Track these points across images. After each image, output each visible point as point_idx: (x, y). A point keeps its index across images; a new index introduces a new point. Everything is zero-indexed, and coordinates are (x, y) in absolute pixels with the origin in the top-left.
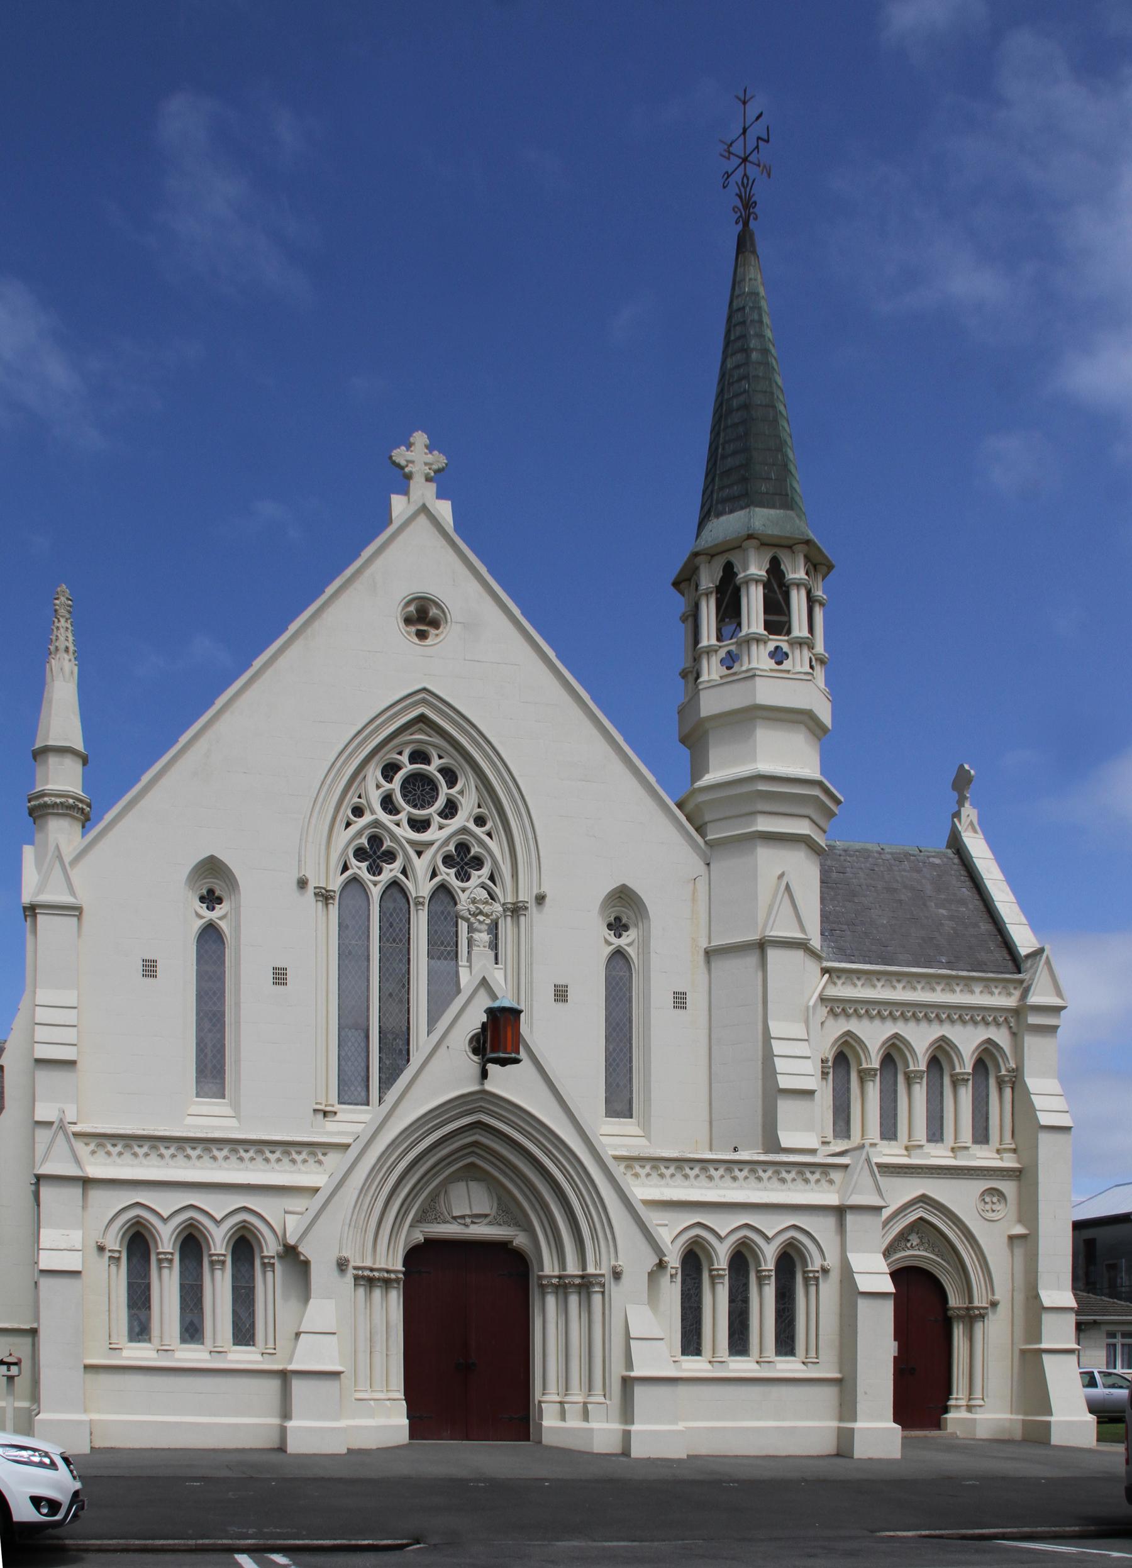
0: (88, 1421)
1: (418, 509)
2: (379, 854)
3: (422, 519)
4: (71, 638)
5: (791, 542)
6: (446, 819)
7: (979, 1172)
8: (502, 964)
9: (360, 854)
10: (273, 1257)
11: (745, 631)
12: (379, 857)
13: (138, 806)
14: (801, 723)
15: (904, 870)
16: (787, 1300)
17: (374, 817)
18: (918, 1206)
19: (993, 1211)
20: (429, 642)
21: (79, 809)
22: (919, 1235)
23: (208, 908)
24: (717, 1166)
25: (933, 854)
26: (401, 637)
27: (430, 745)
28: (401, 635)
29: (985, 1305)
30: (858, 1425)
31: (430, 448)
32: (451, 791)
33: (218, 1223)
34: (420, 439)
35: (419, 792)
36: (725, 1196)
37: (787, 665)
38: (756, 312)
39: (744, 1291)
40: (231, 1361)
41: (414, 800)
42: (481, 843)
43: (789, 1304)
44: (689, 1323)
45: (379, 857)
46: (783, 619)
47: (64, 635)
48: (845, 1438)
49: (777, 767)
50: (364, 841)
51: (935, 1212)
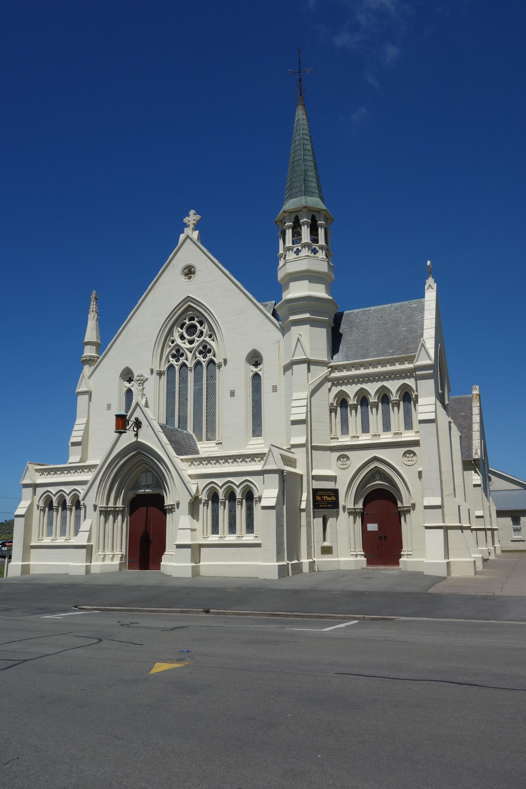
2: (179, 355)
3: (188, 240)
9: (174, 356)
12: (179, 356)
16: (251, 510)
17: (176, 342)
19: (411, 461)
22: (380, 474)
28: (195, 279)
29: (408, 505)
30: (31, 563)
31: (188, 216)
33: (221, 487)
35: (192, 331)
37: (317, 255)
44: (215, 521)
47: (93, 306)
48: (88, 568)
50: (201, 348)
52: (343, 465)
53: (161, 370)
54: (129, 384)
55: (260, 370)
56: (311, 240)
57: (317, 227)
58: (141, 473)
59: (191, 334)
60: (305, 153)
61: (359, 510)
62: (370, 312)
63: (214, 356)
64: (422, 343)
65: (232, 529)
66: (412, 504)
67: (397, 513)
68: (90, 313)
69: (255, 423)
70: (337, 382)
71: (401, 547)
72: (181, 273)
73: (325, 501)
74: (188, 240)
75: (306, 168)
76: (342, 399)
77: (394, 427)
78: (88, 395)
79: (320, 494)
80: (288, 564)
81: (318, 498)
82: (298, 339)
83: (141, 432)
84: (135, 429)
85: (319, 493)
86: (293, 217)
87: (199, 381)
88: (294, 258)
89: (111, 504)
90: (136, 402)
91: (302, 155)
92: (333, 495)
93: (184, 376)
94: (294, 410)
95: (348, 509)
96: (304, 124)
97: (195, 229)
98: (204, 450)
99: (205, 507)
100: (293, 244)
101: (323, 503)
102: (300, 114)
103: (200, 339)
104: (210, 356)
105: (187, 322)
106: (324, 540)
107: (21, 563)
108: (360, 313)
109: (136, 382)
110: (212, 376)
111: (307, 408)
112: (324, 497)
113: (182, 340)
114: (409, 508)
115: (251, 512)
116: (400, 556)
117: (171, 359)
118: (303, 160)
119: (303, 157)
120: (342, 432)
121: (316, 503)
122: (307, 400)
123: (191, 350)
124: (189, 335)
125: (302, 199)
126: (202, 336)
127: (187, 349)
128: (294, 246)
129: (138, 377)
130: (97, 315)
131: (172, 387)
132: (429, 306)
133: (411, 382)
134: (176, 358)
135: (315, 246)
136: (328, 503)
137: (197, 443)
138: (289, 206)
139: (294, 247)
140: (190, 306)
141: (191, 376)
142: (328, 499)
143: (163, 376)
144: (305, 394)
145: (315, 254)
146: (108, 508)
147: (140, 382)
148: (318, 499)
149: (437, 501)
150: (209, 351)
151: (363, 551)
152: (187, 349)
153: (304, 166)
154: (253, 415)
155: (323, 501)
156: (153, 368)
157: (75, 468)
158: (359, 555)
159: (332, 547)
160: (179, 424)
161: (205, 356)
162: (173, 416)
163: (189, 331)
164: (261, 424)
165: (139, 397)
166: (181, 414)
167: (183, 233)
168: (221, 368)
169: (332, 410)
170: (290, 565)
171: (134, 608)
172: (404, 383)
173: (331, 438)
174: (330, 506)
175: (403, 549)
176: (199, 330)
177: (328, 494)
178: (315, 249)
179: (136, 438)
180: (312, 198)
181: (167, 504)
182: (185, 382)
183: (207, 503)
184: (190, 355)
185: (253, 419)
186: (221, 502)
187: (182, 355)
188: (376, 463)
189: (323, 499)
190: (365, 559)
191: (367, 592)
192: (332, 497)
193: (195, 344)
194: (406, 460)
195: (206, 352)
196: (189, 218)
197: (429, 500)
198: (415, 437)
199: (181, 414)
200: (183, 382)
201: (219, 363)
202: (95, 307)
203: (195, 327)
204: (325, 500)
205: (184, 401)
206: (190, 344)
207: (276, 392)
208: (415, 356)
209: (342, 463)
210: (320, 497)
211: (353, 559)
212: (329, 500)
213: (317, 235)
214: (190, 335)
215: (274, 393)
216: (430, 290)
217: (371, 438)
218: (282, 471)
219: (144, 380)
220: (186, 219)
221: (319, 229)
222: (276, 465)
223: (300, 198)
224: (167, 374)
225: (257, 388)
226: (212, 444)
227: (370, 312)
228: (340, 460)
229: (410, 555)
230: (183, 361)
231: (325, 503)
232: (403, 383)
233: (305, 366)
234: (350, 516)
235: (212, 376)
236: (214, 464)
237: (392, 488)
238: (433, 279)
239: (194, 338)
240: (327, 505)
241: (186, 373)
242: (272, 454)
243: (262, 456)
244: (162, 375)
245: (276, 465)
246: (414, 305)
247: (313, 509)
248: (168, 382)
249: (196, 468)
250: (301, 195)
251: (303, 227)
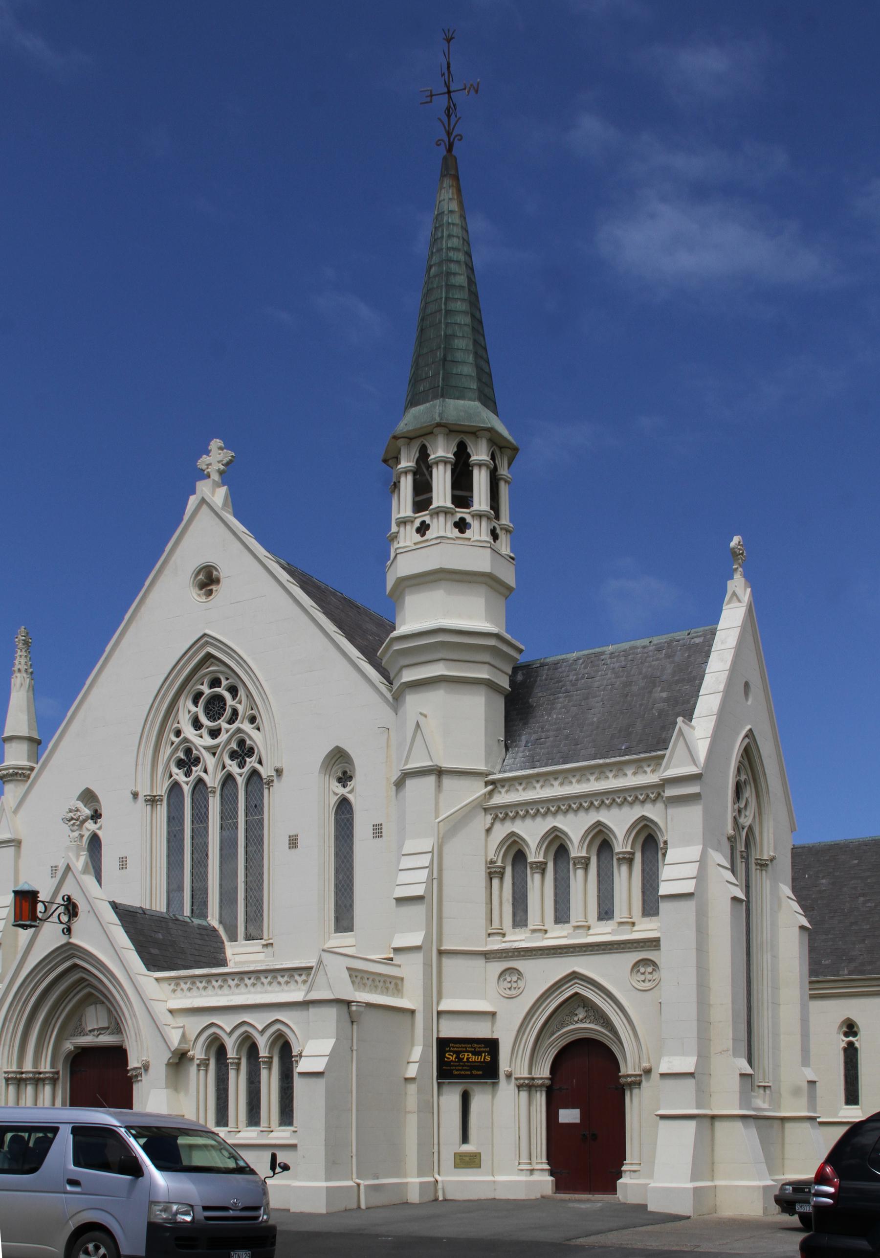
0: (691, 1188)
1: (199, 503)
2: (192, 761)
4: (17, 662)
7: (629, 945)
9: (180, 764)
13: (50, 764)
14: (440, 580)
18: (573, 982)
19: (650, 981)
21: (20, 774)
22: (586, 1008)
24: (233, 977)
27: (219, 672)
29: (637, 1072)
33: (262, 1032)
34: (215, 444)
37: (468, 533)
47: (21, 660)
51: (589, 986)
52: (510, 989)
53: (155, 794)
54: (94, 825)
55: (350, 792)
56: (453, 503)
57: (470, 468)
59: (214, 715)
60: (451, 296)
61: (540, 1082)
62: (603, 657)
63: (260, 762)
64: (680, 728)
65: (254, 1117)
66: (643, 1070)
68: (14, 676)
69: (340, 902)
70: (505, 813)
72: (191, 585)
73: (466, 1064)
74: (205, 508)
75: (449, 332)
77: (620, 911)
79: (455, 1049)
80: (359, 1185)
81: (449, 1057)
82: (418, 725)
83: (76, 926)
84: (64, 918)
85: (453, 1047)
87: (231, 817)
88: (415, 544)
89: (28, 1066)
90: (66, 865)
91: (442, 301)
92: (485, 1052)
93: (201, 807)
94: (403, 877)
95: (516, 1079)
96: (453, 224)
97: (217, 485)
98: (238, 958)
99: (202, 1073)
101: (460, 1068)
102: (444, 200)
104: (251, 762)
105: (207, 691)
106: (465, 1139)
107: (691, 1185)
108: (581, 661)
109: (67, 822)
110: (256, 806)
111: (431, 872)
112: (464, 1055)
113: (197, 730)
114: (638, 1078)
116: (619, 1175)
117: (175, 770)
118: (443, 312)
119: (445, 304)
120: (514, 921)
121: (444, 1068)
122: (431, 854)
124: (210, 717)
125: (435, 406)
126: (237, 719)
127: (205, 748)
129: (70, 812)
130: (28, 680)
131: (177, 829)
132: (722, 643)
133: (652, 812)
134: (185, 769)
135: (461, 513)
136: (473, 1066)
137: (227, 944)
138: (406, 424)
139: (416, 518)
140: (209, 656)
141: (214, 805)
142: (474, 1058)
143: (159, 806)
144: (427, 843)
145: (462, 531)
146: (22, 1073)
147: (74, 823)
148: (449, 1058)
149: (687, 1064)
150: (251, 752)
151: (548, 1164)
152: (205, 748)
153: (446, 327)
154: (336, 886)
155: (461, 1064)
156: (139, 789)
158: (537, 1170)
159: (480, 1154)
160: (192, 906)
161: (241, 763)
162: (181, 889)
163: (211, 710)
164: (351, 906)
165: (70, 854)
166: (196, 885)
167: (194, 493)
168: (271, 788)
169: (494, 873)
170: (362, 1188)
172: (643, 816)
173: (489, 934)
174: (478, 1073)
176: (230, 706)
177: (473, 1049)
178: (462, 520)
179: (68, 936)
180: (462, 402)
181: (132, 1067)
182: (203, 817)
183: (204, 1064)
184: (210, 761)
185: (336, 894)
186: (264, 1062)
187: (197, 761)
188: (577, 985)
189: (460, 1060)
190: (551, 1178)
191: (445, 1238)
192: (483, 1054)
193: (223, 737)
194: (638, 979)
196: (208, 458)
197: (670, 1062)
198: (568, 939)
199: (196, 885)
200: (199, 818)
201: (268, 776)
202: (23, 661)
203: (220, 699)
204: (465, 1060)
205: (201, 858)
206: (213, 739)
207: (380, 839)
208: (663, 757)
209: (643, 977)
210: (454, 1056)
211: (523, 1178)
212: (475, 1062)
213: (470, 488)
214: (212, 717)
215: (377, 840)
216: (735, 604)
217: (568, 934)
218: (348, 1003)
219: (81, 818)
220: (203, 462)
221: (476, 472)
222: (331, 990)
223: (431, 403)
224: (222, 795)
225: (346, 829)
226: (255, 946)
227: (603, 657)
228: (505, 979)
229: (635, 1171)
230: (198, 775)
231: (466, 1068)
233: (431, 780)
234: (521, 1093)
235: (256, 806)
236: (218, 988)
239: (220, 724)
240: (471, 1070)
241: (205, 799)
242: (324, 968)
244: (157, 805)
245: (331, 990)
246: (697, 640)
247: (437, 1079)
248: (170, 819)
249: (186, 997)
250: (435, 397)
251: (434, 471)
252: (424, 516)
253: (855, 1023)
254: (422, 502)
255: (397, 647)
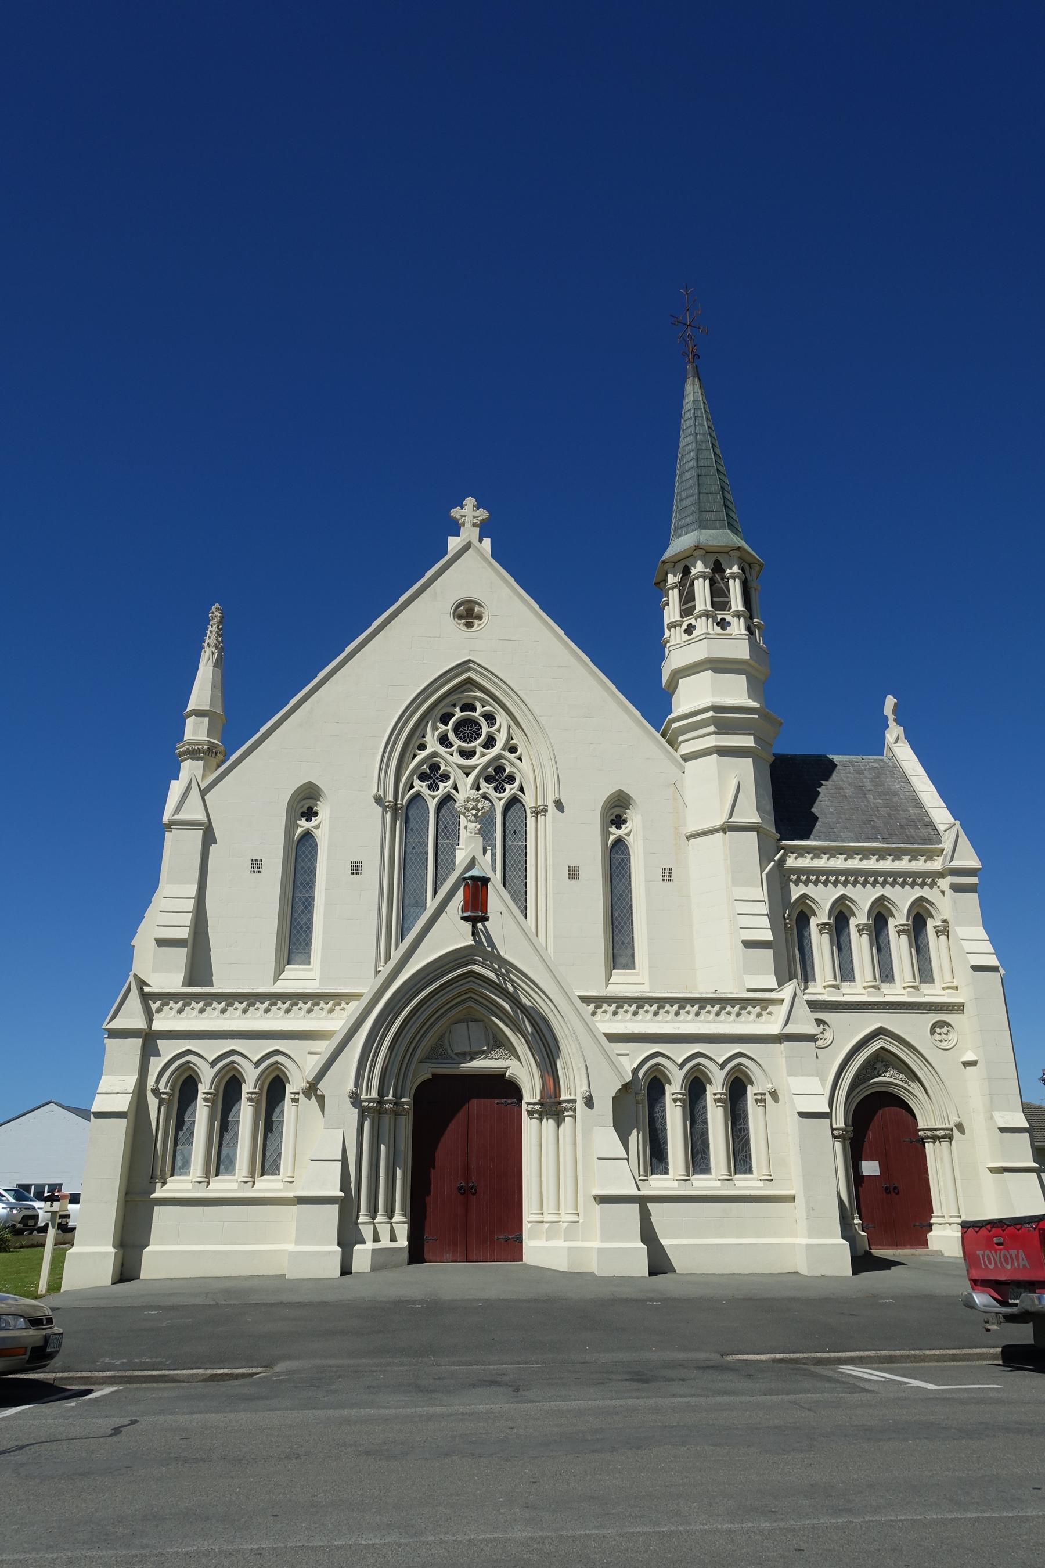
5: (726, 550)
6: (488, 749)
8: (463, 845)
10: (298, 1093)
11: (734, 609)
15: (850, 773)
16: (742, 1121)
20: (473, 629)
22: (884, 1063)
23: (307, 820)
25: (872, 760)
26: (455, 628)
32: (491, 730)
34: (470, 502)
35: (468, 731)
36: (679, 1028)
37: (729, 630)
38: (699, 411)
39: (703, 1113)
40: (740, 1188)
41: (465, 737)
42: (512, 764)
43: (745, 1125)
45: (437, 778)
46: (726, 600)
47: (212, 635)
49: (726, 700)
58: (454, 1024)
67: (913, 1141)
71: (929, 1209)
76: (877, 913)
78: (202, 831)
86: (680, 566)
88: (685, 642)
93: (448, 823)
100: (682, 617)
103: (489, 751)
107: (805, 1241)
110: (515, 832)
115: (742, 1126)
116: (929, 1227)
123: (467, 771)
128: (684, 620)
134: (429, 782)
139: (683, 622)
145: (723, 629)
157: (251, 999)
171: (898, 1353)
175: (933, 1213)
182: (450, 834)
195: (503, 780)
232: (802, 892)
235: (515, 832)
237: (857, 1092)
238: (902, 727)
243: (325, 999)
252: (690, 620)
253: (630, 797)
254: (687, 598)
255: (674, 725)
